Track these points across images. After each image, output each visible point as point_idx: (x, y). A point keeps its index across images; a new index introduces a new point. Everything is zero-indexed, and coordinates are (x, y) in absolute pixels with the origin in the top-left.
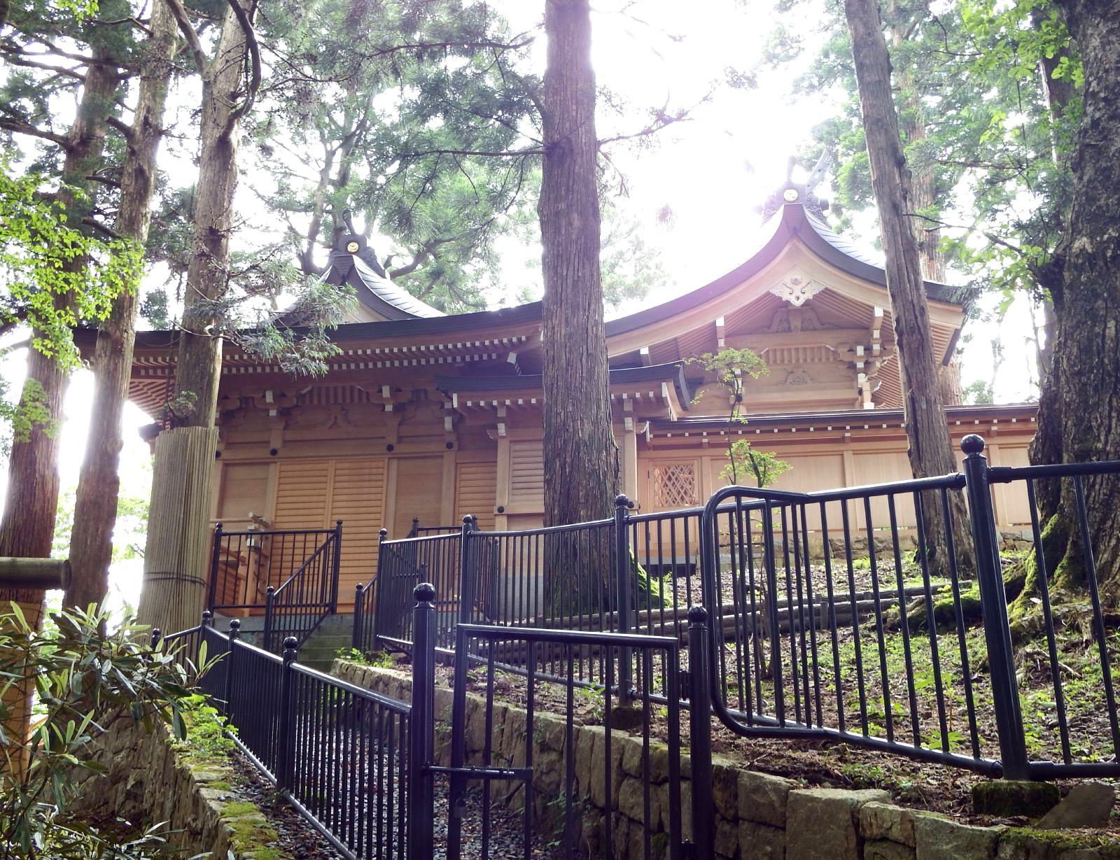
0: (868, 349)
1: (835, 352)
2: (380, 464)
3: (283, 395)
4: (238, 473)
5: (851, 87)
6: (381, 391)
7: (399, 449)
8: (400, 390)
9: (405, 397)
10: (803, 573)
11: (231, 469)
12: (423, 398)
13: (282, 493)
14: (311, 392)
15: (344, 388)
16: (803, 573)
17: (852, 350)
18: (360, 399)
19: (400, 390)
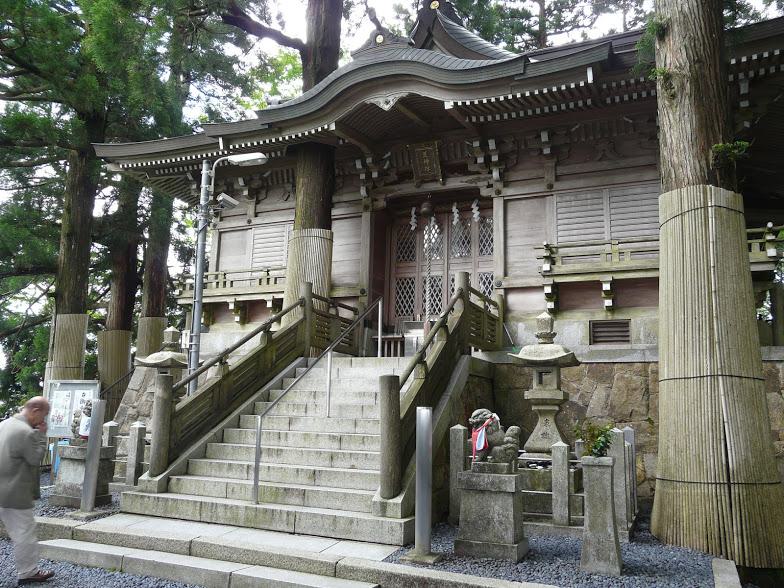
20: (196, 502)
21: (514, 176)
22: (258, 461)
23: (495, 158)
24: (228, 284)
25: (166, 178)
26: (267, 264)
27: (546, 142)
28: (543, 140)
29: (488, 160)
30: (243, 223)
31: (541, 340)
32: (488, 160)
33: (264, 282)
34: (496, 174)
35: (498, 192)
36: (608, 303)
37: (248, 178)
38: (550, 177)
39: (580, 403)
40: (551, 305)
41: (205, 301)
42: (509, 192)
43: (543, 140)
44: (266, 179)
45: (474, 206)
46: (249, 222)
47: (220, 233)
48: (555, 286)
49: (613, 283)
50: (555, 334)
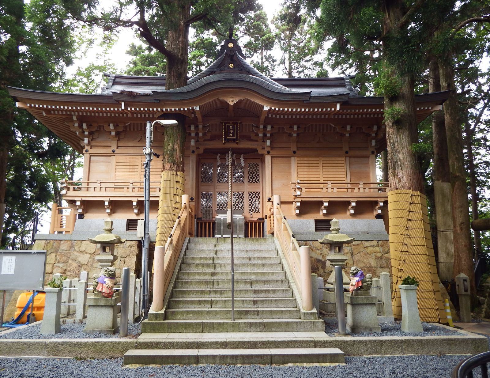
0: (197, 127)
1: (334, 128)
2: (343, 159)
3: (118, 126)
4: (274, 159)
5: (100, 94)
6: (109, 126)
7: (351, 153)
8: (91, 125)
9: (120, 129)
10: (260, 262)
11: (273, 158)
12: (102, 129)
13: (117, 170)
14: (130, 125)
15: (141, 124)
16: (260, 262)
17: (292, 127)
18: (330, 130)
19: (91, 125)
20: (311, 322)
21: (93, 143)
22: (233, 297)
23: (269, 135)
24: (103, 189)
25: (54, 116)
26: (133, 179)
27: (269, 131)
28: (348, 130)
29: (265, 135)
30: (109, 151)
31: (106, 232)
32: (265, 135)
33: (98, 189)
34: (268, 143)
35: (268, 152)
36: (325, 211)
37: (116, 124)
38: (114, 147)
39: (323, 260)
40: (298, 211)
41: (151, 199)
42: (91, 151)
43: (192, 129)
44: (127, 126)
45: (241, 158)
46: (114, 151)
47: (91, 156)
48: (302, 203)
49: (329, 203)
50: (112, 229)
